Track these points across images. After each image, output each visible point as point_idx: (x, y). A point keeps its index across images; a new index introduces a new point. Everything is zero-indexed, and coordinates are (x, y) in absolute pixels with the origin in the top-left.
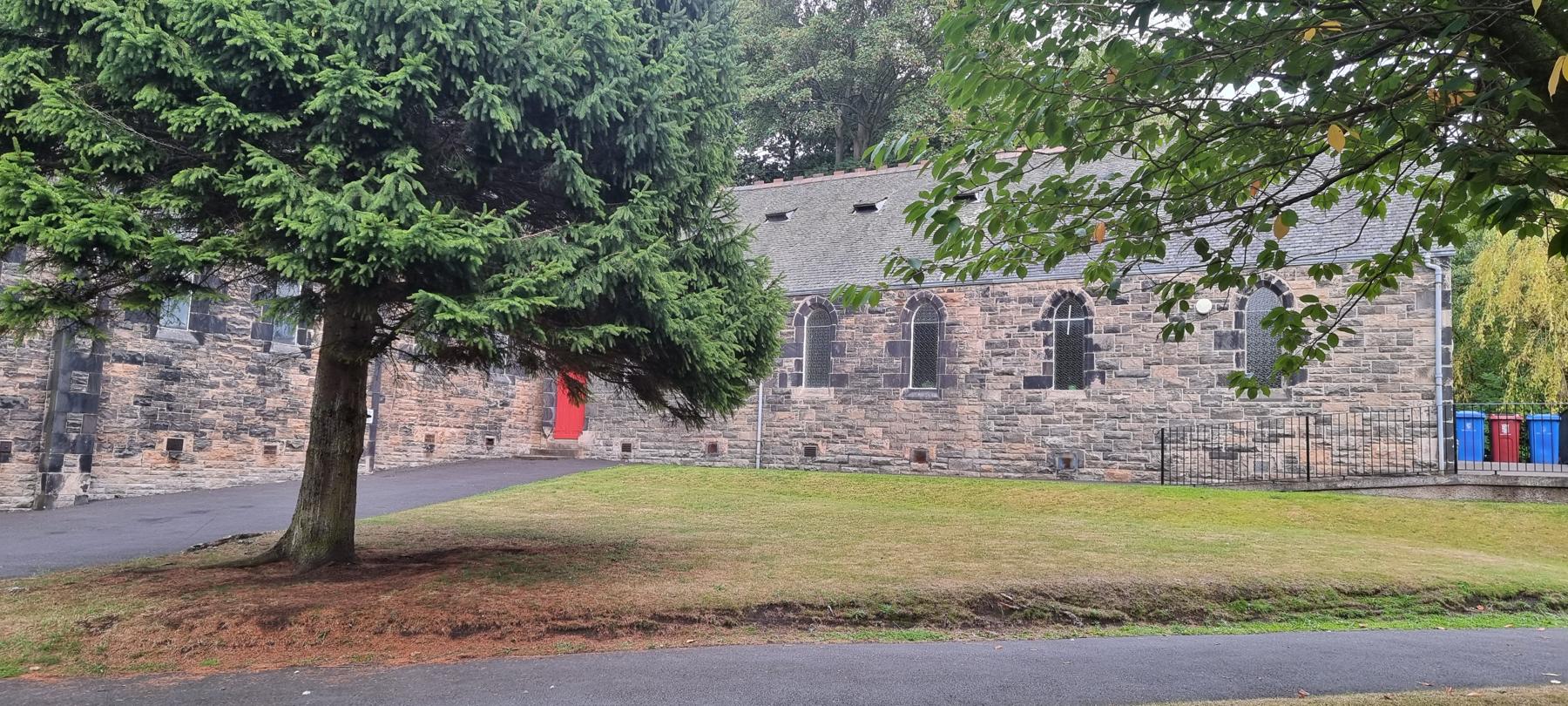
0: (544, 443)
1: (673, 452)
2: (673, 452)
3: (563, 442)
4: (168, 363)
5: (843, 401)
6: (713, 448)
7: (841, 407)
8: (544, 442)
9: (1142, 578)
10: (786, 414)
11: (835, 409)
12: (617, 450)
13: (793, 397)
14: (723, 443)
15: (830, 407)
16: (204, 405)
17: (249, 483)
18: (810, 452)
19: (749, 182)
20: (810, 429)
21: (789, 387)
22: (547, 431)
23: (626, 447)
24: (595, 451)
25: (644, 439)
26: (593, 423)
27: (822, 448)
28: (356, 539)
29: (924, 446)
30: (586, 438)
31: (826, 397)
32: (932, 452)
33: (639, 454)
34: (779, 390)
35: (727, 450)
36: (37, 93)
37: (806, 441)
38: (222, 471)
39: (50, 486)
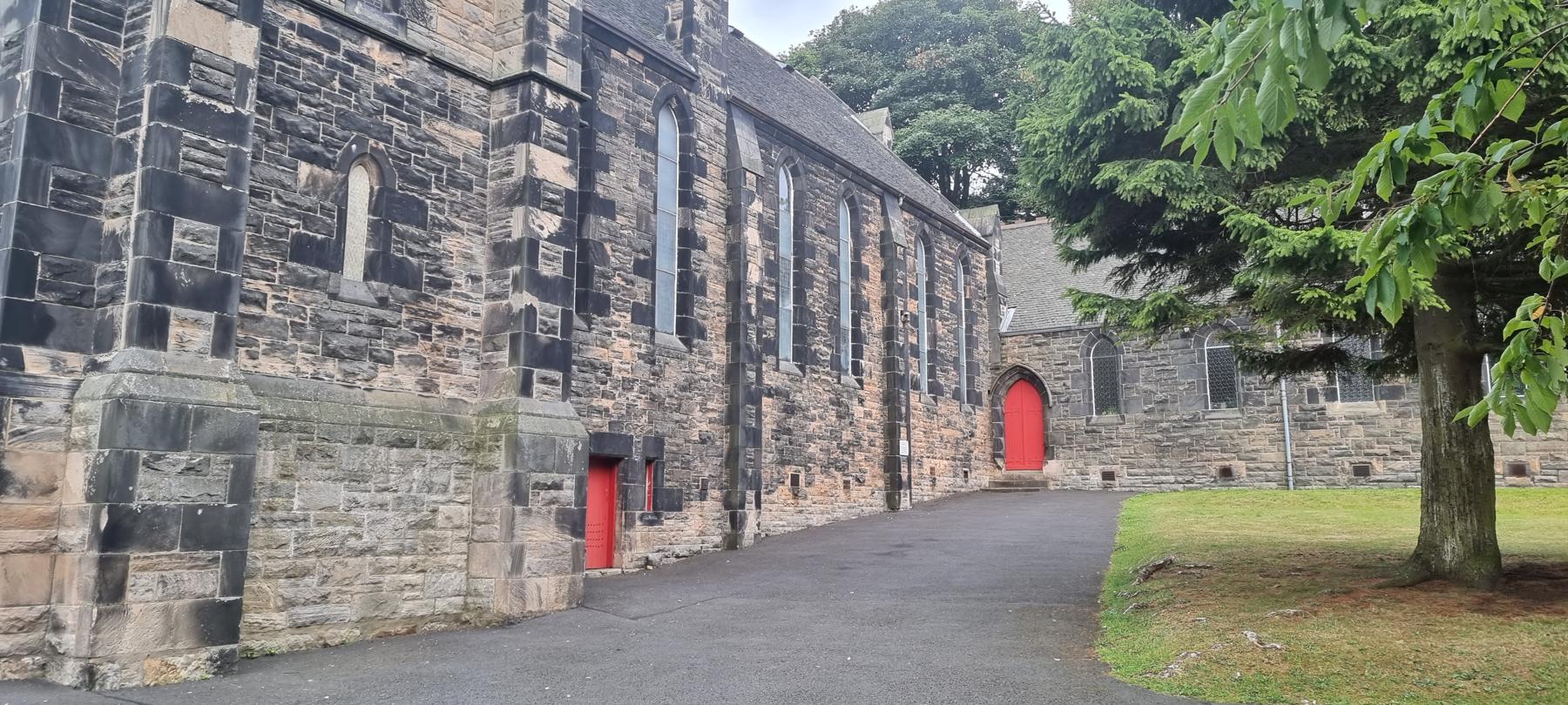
0: (1000, 475)
1: (1172, 478)
2: (1172, 478)
3: (1016, 473)
4: (787, 396)
5: (1400, 415)
6: (1226, 473)
7: (1399, 422)
8: (998, 474)
9: (247, 677)
10: (1322, 432)
11: (1390, 424)
12: (1096, 479)
13: (1329, 413)
14: (1239, 467)
15: (1383, 422)
16: (809, 438)
17: (836, 520)
18: (1362, 471)
19: (1033, 219)
20: (1359, 447)
21: (1322, 402)
22: (1000, 462)
23: (1108, 476)
24: (1067, 480)
25: (1131, 466)
26: (1059, 451)
27: (1378, 466)
28: (1500, 544)
29: (1523, 458)
30: (1052, 467)
31: (1376, 411)
32: (1534, 464)
33: (1127, 483)
34: (1308, 406)
35: (1244, 473)
36: (1148, 58)
37: (1354, 459)
38: (822, 507)
39: (736, 522)
